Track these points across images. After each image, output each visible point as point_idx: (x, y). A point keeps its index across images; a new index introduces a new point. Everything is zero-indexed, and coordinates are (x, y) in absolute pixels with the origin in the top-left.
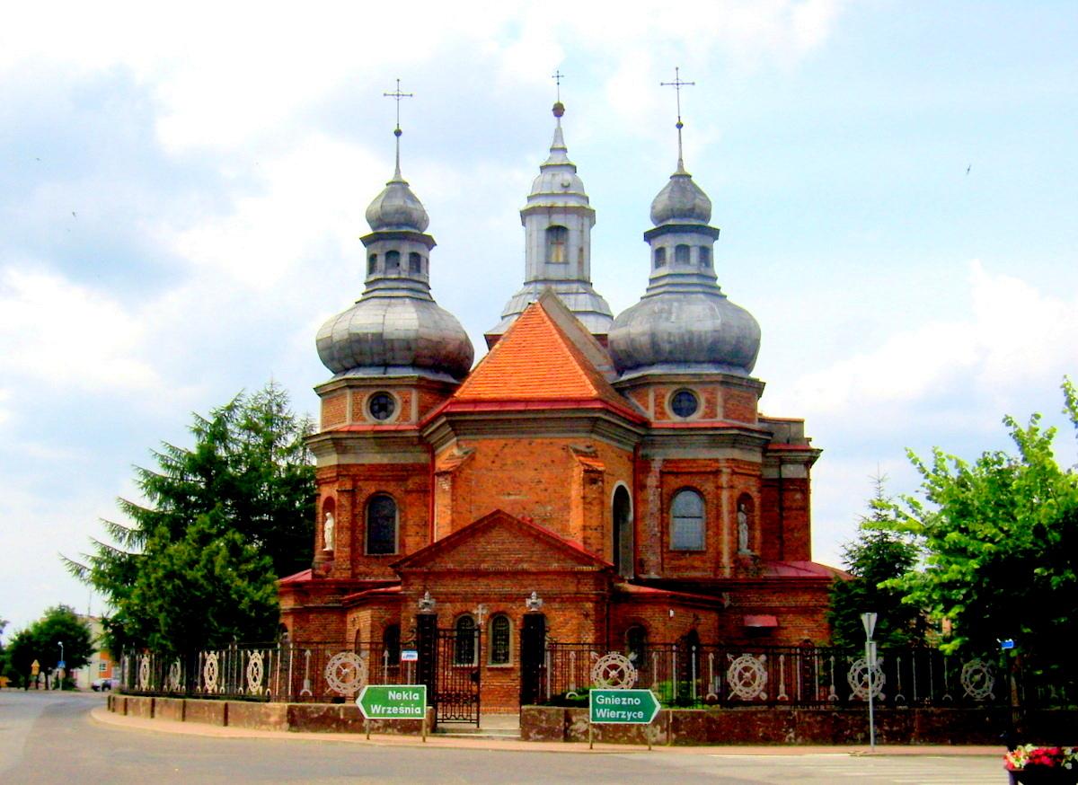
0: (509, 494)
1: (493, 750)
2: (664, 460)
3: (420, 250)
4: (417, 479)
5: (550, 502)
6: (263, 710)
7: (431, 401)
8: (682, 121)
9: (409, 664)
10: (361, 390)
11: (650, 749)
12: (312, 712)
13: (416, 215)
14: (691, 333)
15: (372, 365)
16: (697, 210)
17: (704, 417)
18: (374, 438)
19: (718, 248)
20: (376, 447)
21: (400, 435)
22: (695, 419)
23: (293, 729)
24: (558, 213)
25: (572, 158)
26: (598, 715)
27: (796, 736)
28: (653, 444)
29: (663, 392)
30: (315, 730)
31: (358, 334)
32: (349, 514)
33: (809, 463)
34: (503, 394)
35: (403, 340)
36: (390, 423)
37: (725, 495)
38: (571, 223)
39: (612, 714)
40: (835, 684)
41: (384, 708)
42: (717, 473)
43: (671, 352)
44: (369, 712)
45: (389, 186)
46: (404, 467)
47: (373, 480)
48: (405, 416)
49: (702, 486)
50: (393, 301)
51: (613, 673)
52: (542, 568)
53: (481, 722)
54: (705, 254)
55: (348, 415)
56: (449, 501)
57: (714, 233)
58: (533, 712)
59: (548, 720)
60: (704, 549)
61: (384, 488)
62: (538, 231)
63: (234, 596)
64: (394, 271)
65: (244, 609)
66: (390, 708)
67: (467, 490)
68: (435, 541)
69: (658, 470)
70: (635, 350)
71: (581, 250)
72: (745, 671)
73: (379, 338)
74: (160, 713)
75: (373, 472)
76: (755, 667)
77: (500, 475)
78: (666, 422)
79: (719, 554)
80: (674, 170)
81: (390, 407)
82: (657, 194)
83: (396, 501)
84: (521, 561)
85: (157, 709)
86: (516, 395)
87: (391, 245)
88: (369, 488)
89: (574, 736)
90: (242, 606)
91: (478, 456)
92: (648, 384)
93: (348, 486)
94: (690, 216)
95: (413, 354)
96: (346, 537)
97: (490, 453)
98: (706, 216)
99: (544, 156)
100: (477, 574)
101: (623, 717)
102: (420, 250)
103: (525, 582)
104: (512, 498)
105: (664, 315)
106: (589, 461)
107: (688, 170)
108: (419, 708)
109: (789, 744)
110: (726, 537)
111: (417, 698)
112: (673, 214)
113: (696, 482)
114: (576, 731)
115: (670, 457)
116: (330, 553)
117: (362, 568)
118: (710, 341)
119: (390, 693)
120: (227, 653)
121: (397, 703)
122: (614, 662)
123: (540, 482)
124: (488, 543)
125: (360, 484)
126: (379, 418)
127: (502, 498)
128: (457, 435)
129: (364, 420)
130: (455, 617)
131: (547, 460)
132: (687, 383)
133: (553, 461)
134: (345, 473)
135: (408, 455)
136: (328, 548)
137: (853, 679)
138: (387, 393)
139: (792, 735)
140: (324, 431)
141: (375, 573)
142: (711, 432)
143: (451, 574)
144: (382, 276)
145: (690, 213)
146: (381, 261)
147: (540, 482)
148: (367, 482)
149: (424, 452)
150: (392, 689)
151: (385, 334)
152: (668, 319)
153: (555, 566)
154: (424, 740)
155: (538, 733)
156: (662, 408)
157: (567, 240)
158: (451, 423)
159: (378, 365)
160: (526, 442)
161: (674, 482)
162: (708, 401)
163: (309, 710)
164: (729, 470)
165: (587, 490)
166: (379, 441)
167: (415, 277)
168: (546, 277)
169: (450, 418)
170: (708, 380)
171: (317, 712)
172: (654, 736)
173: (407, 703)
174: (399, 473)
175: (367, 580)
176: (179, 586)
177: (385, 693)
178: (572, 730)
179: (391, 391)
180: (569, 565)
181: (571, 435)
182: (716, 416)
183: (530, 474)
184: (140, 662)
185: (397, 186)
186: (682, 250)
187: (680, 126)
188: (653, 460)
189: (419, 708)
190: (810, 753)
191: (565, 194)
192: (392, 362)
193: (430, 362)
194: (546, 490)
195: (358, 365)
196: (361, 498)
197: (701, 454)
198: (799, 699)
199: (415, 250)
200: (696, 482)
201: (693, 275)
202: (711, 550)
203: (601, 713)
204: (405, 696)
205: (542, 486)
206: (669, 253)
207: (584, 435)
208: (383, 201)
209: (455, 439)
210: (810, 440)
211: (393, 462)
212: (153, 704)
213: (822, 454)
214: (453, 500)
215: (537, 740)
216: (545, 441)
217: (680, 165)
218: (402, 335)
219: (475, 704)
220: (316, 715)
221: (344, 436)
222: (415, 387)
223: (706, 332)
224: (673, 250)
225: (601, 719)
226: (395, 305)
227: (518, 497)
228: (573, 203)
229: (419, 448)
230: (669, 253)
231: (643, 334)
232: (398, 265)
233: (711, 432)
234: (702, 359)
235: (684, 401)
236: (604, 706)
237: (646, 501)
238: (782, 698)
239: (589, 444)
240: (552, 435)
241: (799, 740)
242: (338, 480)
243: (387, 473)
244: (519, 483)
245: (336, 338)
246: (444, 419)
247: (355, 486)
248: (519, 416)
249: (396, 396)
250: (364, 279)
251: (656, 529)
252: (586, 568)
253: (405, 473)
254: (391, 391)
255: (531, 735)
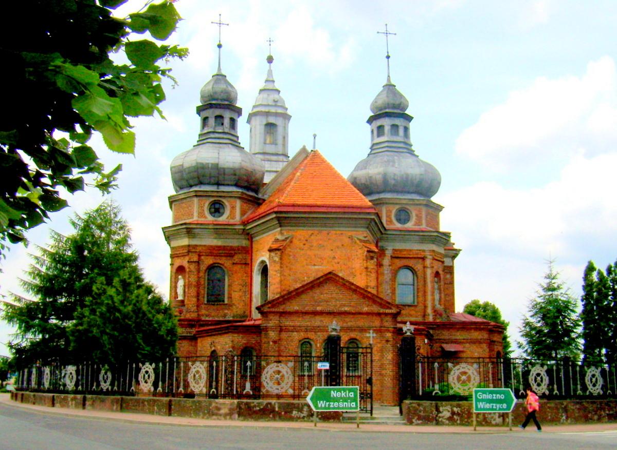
0: (315, 265)
1: (416, 433)
2: (393, 249)
3: (235, 116)
4: (240, 256)
5: (341, 270)
6: (214, 405)
7: (247, 208)
8: (389, 55)
9: (323, 372)
10: (204, 198)
11: (511, 430)
12: (255, 406)
13: (233, 95)
14: (407, 175)
15: (209, 184)
16: (402, 105)
17: (415, 225)
18: (214, 229)
19: (412, 125)
20: (215, 235)
21: (231, 227)
22: (410, 225)
23: (241, 418)
24: (271, 116)
25: (277, 86)
26: (479, 407)
27: (567, 418)
28: (387, 240)
29: (391, 209)
30: (257, 419)
31: (202, 164)
32: (196, 276)
33: (454, 257)
34: (310, 201)
35: (232, 169)
36: (223, 219)
37: (429, 272)
38: (279, 121)
39: (488, 406)
40: (523, 385)
41: (327, 403)
42: (423, 259)
43: (394, 185)
44: (316, 406)
45: (215, 78)
46: (232, 248)
47: (211, 256)
48: (232, 215)
49: (415, 266)
50: (221, 145)
51: (464, 378)
52: (357, 310)
53: (374, 412)
54: (406, 129)
55: (196, 214)
56: (279, 268)
57: (409, 118)
58: (414, 405)
59: (425, 411)
60: (416, 304)
61: (218, 261)
62: (260, 125)
63: (156, 325)
64: (220, 128)
65: (163, 335)
66: (332, 403)
67: (288, 261)
68: (270, 296)
69: (390, 255)
70: (371, 183)
71: (284, 138)
72: (462, 375)
73: (216, 167)
74: (92, 405)
75: (213, 251)
76: (470, 372)
77: (309, 252)
78: (391, 227)
79: (425, 307)
80: (385, 82)
81: (221, 211)
82: (377, 94)
83: (225, 270)
84: (344, 305)
85: (88, 403)
86: (319, 203)
87: (218, 112)
88: (209, 261)
89: (441, 421)
90: (161, 333)
91: (295, 241)
92: (383, 203)
93: (196, 259)
94: (398, 109)
95: (237, 177)
96: (193, 291)
97: (302, 239)
98: (405, 108)
99: (262, 85)
100: (315, 313)
101: (494, 407)
102: (235, 116)
103: (346, 319)
104: (316, 267)
105: (391, 164)
106: (368, 245)
107: (393, 82)
108: (354, 403)
109: (563, 424)
110: (429, 297)
111: (353, 396)
112: (388, 106)
113: (406, 262)
114: (443, 417)
115: (397, 248)
116: (183, 301)
117: (203, 312)
118: (418, 180)
119: (332, 392)
120: (164, 365)
121: (336, 400)
122: (463, 370)
123: (334, 258)
124: (322, 294)
125: (203, 257)
126: (214, 216)
127: (310, 267)
128: (281, 226)
129: (205, 217)
130: (300, 341)
131: (339, 244)
132: (406, 204)
133: (343, 245)
134: (193, 250)
135: (235, 240)
136: (180, 298)
137: (453, 379)
138: (220, 201)
139: (564, 417)
140: (175, 224)
141: (213, 315)
142: (421, 234)
143: (290, 313)
144: (212, 130)
145: (394, 107)
146: (212, 121)
147: (334, 258)
148: (207, 257)
149: (245, 239)
150: (334, 390)
151: (220, 163)
152: (393, 166)
153: (365, 309)
154: (315, 425)
155: (419, 419)
156: (390, 218)
157: (276, 131)
158: (278, 219)
159: (213, 184)
160: (326, 232)
161: (399, 263)
162: (417, 215)
163: (252, 405)
164: (431, 257)
165: (368, 263)
166: (216, 230)
167: (232, 132)
168: (264, 151)
169: (278, 215)
170: (417, 203)
171: (258, 406)
172: (494, 420)
173: (345, 400)
174: (229, 252)
175: (207, 319)
176: (118, 317)
177: (329, 392)
178: (440, 417)
179: (224, 200)
180: (375, 309)
181: (354, 229)
182: (422, 225)
183: (327, 253)
184: (44, 372)
185: (220, 77)
186: (395, 127)
187: (388, 57)
188: (387, 249)
189: (354, 403)
190: (591, 430)
191: (276, 106)
192: (223, 183)
193: (246, 184)
194: (338, 263)
195: (201, 183)
196: (203, 267)
197: (414, 246)
198: (564, 394)
199: (232, 116)
200: (410, 263)
201: (400, 142)
202: (421, 305)
203: (481, 405)
204: (343, 394)
205: (336, 261)
206: (387, 129)
207: (363, 229)
208: (213, 84)
209: (279, 229)
210: (454, 244)
211: (225, 245)
212: (84, 399)
213: (461, 252)
214: (281, 267)
215: (417, 425)
216: (338, 232)
217: (389, 80)
218: (231, 166)
219: (369, 400)
220: (258, 408)
221: (194, 226)
222: (239, 198)
223: (416, 175)
224: (389, 127)
225: (481, 409)
226: (224, 148)
227: (320, 267)
228: (280, 111)
229: (243, 237)
230: (387, 129)
231: (379, 174)
232: (223, 124)
233: (421, 234)
234: (411, 191)
235: (403, 215)
236: (482, 400)
237: (383, 274)
238: (213, 392)
239: (365, 235)
240: (342, 229)
241: (569, 421)
242: (188, 255)
243: (221, 252)
244: (321, 258)
245: (186, 165)
246: (274, 216)
247: (199, 259)
248: (325, 216)
249: (227, 203)
250: (199, 132)
251: (389, 291)
252: (388, 311)
253: (233, 252)
254: (224, 200)
255: (414, 420)
